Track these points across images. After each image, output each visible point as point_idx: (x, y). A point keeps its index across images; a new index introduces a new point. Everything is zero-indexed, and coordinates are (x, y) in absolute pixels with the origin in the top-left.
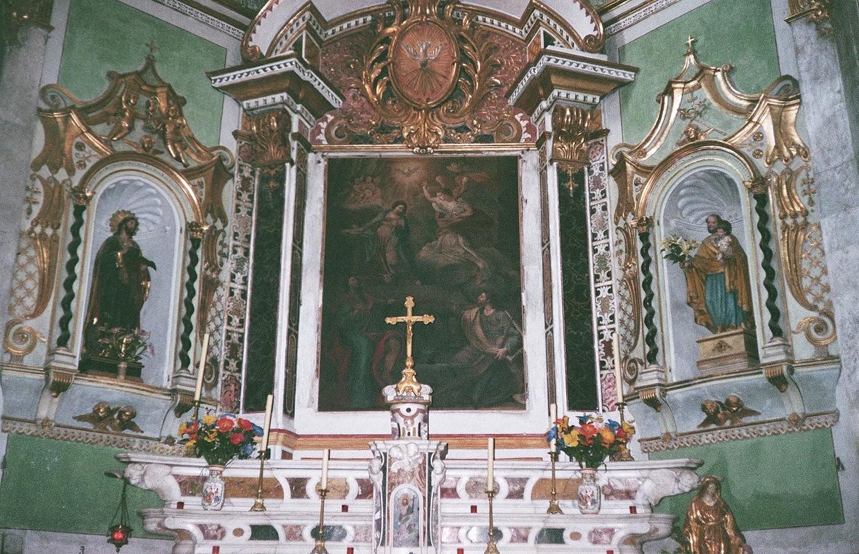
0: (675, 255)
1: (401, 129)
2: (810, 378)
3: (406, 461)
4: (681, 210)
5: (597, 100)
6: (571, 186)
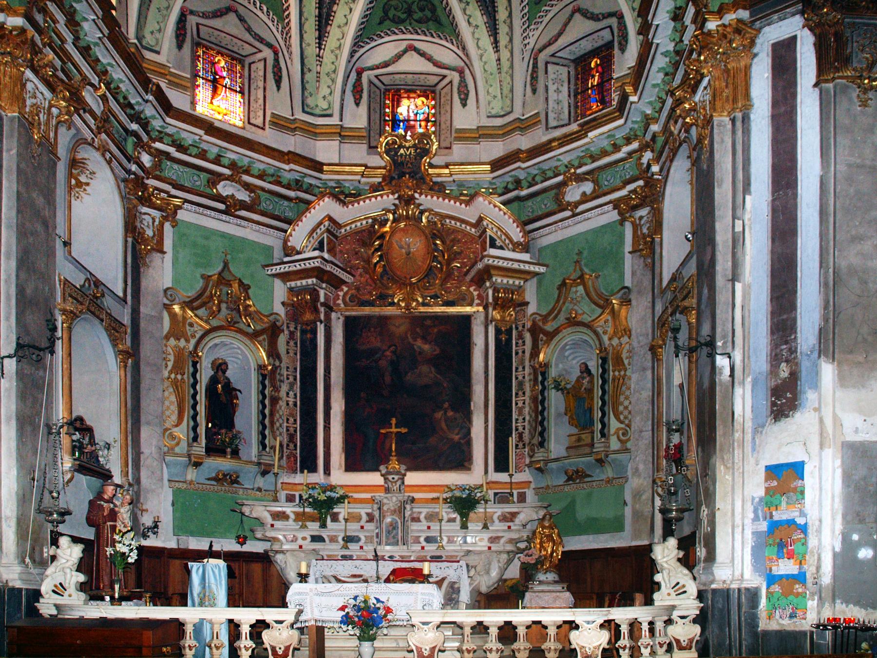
0: (557, 387)
1: (393, 296)
2: (616, 459)
3: (391, 505)
4: (567, 357)
5: (522, 284)
6: (503, 338)
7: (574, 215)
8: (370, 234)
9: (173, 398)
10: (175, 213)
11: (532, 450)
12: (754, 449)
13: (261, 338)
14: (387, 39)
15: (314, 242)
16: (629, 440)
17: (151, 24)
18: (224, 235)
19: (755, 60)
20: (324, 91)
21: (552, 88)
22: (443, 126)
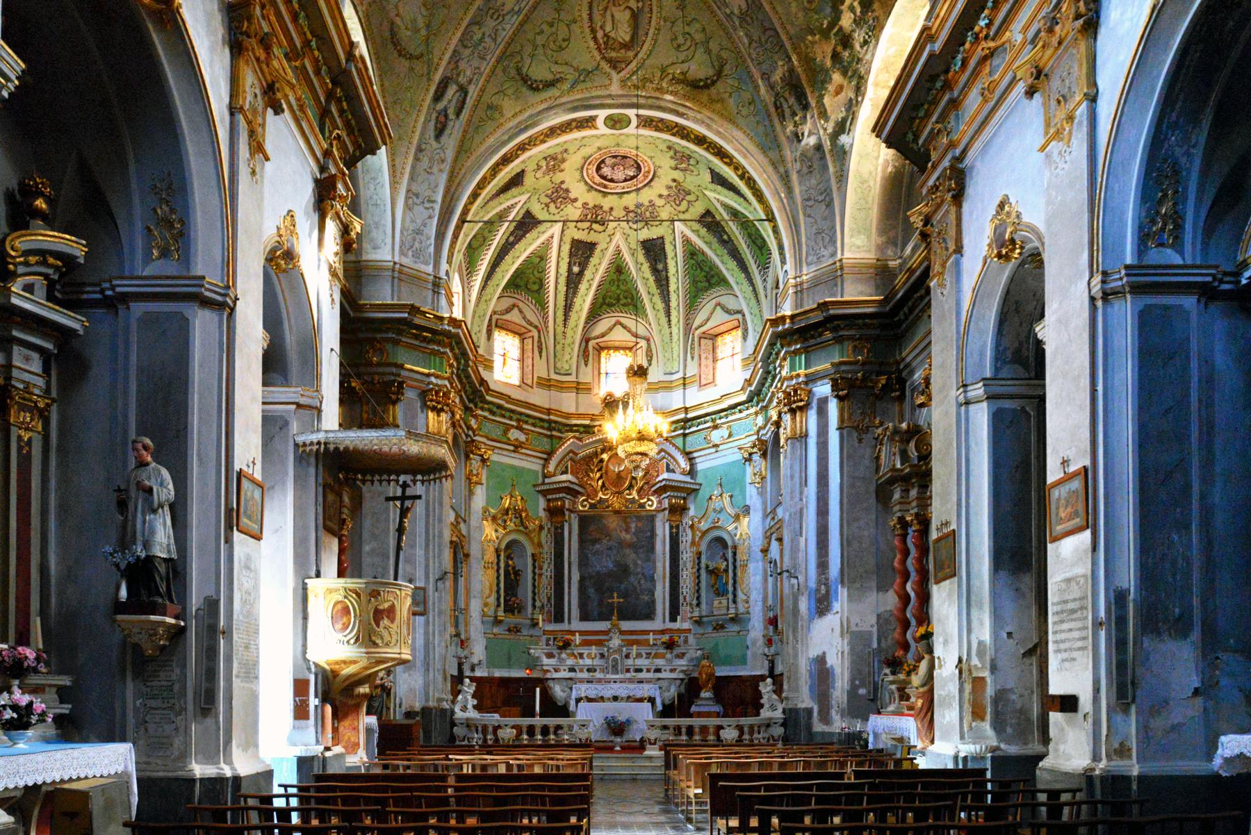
18: (512, 467)
21: (703, 356)
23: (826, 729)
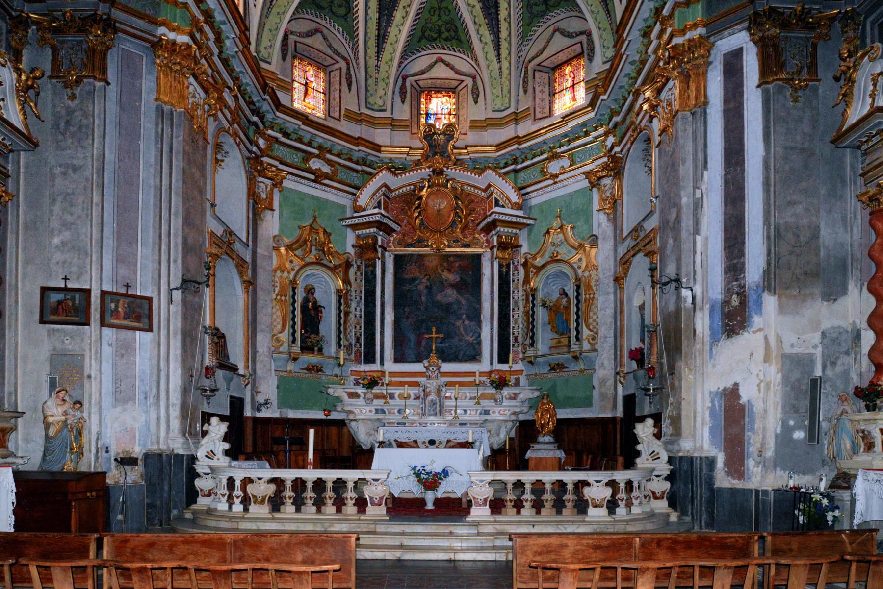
0: (544, 305)
6: (504, 270)
7: (555, 183)
8: (411, 198)
9: (279, 313)
10: (281, 182)
11: (525, 349)
12: (711, 357)
13: (338, 271)
14: (425, 53)
15: (374, 202)
16: (597, 343)
17: (265, 43)
18: (314, 197)
19: (710, 67)
20: (381, 92)
21: (538, 89)
22: (461, 118)
23: (738, 484)
